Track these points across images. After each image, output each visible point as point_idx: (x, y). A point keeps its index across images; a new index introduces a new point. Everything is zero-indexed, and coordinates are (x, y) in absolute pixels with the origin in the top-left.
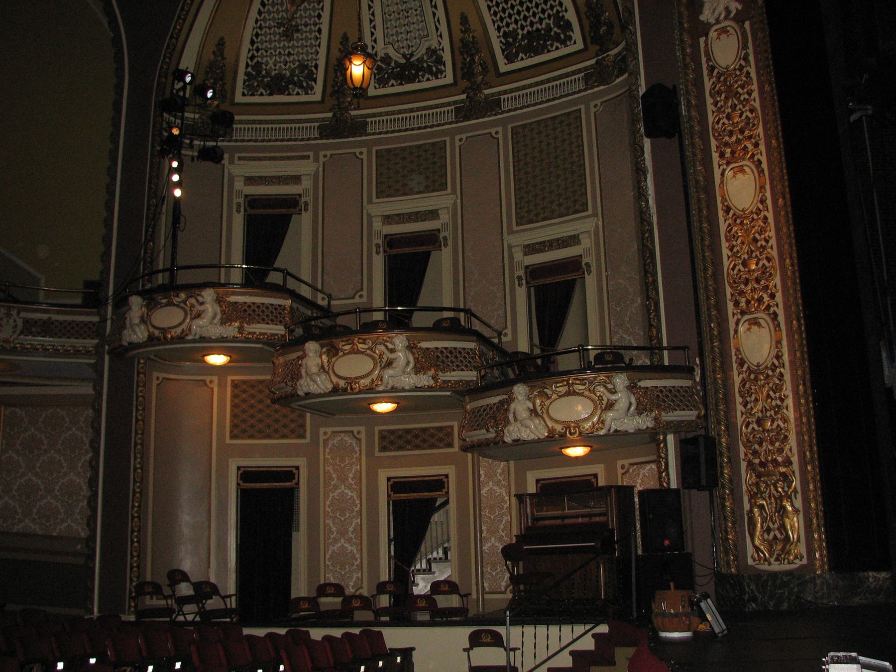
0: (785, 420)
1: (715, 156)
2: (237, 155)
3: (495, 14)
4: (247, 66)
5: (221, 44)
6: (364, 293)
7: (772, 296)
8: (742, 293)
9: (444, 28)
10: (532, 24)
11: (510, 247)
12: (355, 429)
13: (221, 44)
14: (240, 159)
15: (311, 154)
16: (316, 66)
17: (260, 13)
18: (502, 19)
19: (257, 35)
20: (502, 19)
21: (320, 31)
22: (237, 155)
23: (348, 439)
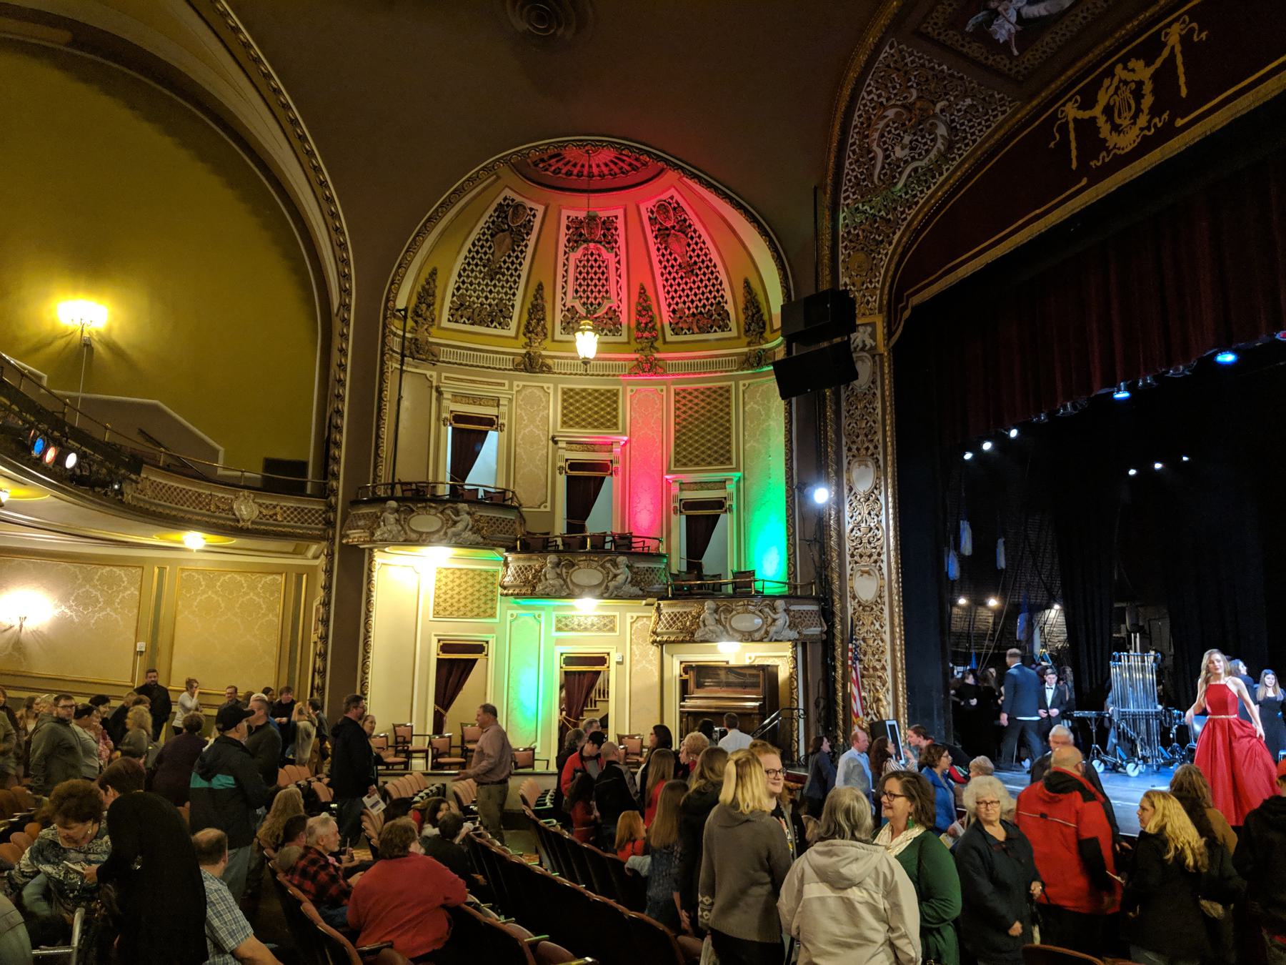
0: (882, 641)
1: (845, 449)
2: (444, 374)
3: (668, 292)
4: (454, 295)
5: (434, 273)
6: (548, 504)
7: (876, 447)
8: (854, 442)
9: (624, 294)
10: (697, 307)
11: (668, 483)
12: (545, 385)
13: (434, 273)
14: (446, 378)
15: (507, 382)
16: (513, 306)
17: (470, 251)
18: (673, 298)
19: (464, 270)
20: (673, 298)
21: (519, 276)
22: (444, 374)
23: (538, 393)
